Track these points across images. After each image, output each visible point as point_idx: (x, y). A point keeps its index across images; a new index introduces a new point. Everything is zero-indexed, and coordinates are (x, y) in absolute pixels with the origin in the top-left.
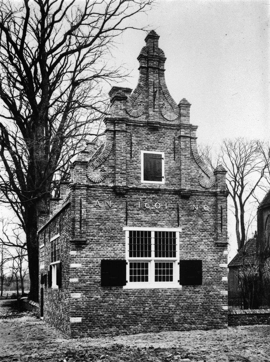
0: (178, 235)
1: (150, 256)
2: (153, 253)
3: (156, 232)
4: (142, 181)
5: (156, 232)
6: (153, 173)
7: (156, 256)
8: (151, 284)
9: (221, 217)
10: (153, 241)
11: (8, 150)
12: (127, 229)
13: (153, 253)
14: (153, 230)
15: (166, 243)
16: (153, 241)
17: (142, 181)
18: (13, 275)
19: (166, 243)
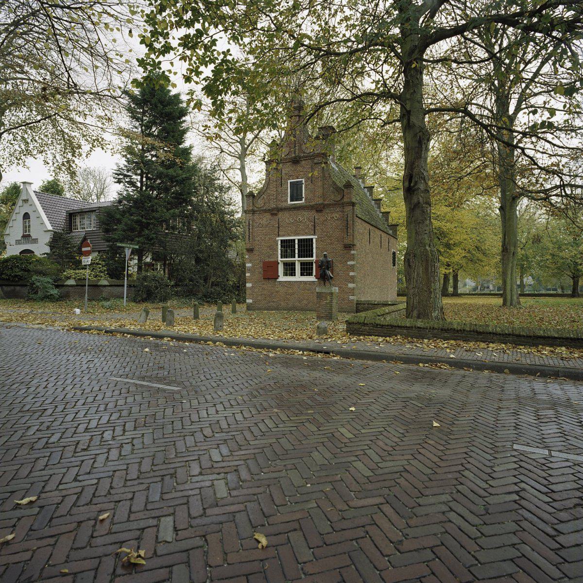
0: (314, 241)
1: (294, 257)
2: (297, 255)
3: (299, 240)
4: (289, 202)
5: (299, 240)
6: (296, 196)
7: (299, 257)
8: (298, 278)
9: (283, 348)
10: (297, 251)
11: (136, 97)
12: (289, 181)
13: (297, 255)
14: (296, 238)
15: (306, 247)
16: (297, 251)
17: (289, 202)
18: (128, 159)
19: (306, 247)
